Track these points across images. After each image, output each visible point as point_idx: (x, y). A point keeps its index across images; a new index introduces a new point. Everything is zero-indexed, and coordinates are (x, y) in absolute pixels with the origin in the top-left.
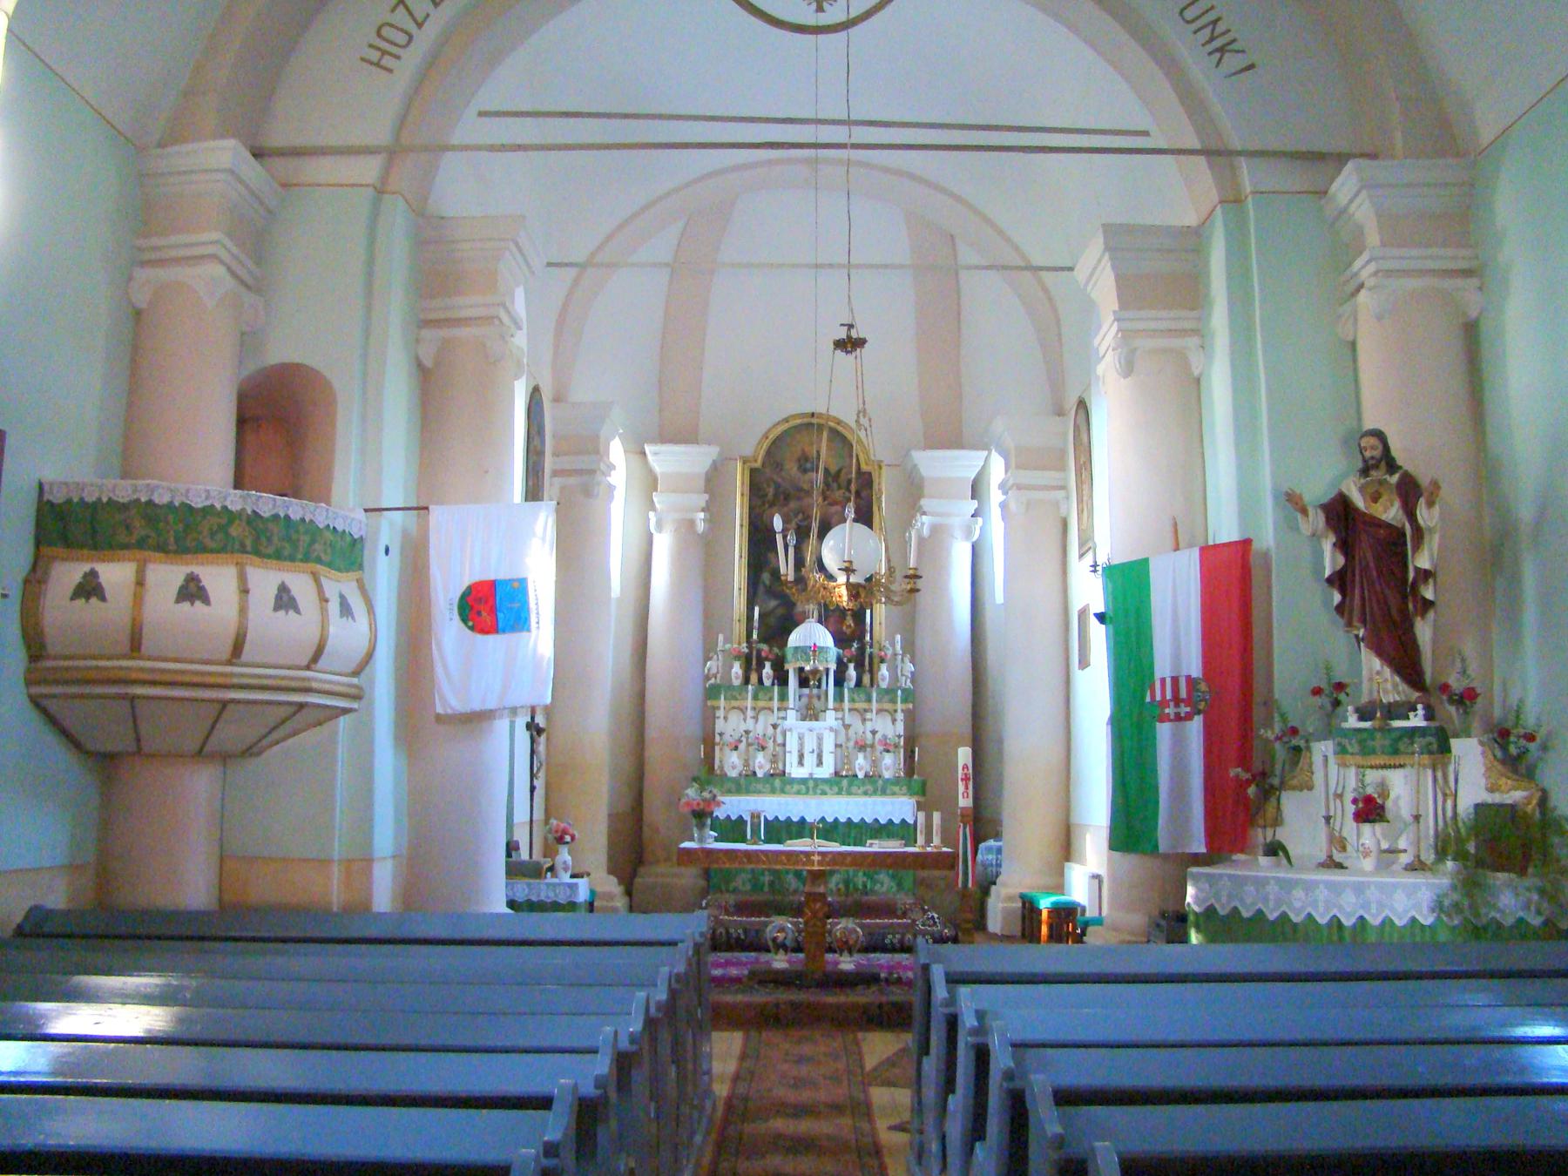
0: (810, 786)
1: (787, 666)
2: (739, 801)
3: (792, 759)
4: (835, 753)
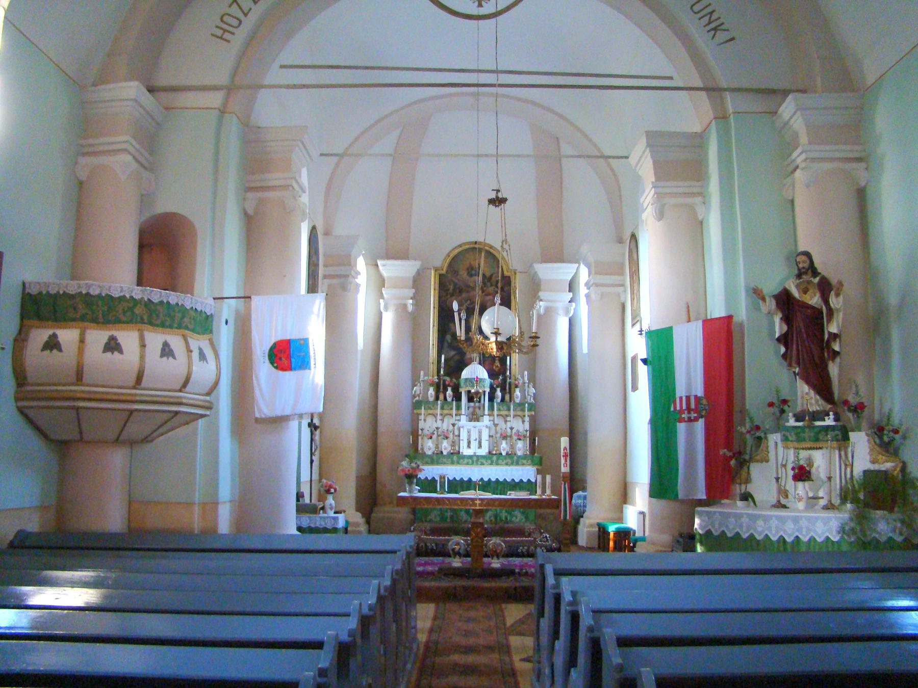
0: (475, 460)
1: (461, 390)
2: (433, 469)
3: (464, 444)
4: (489, 441)
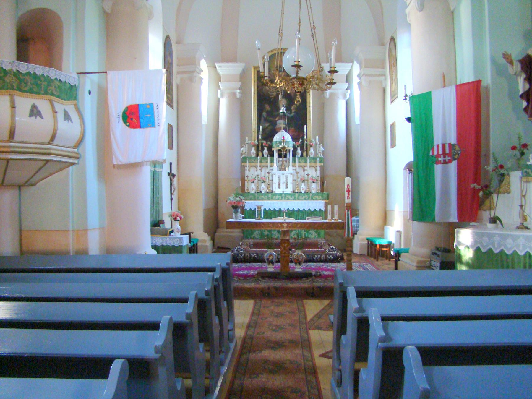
0: (283, 196)
1: (273, 149)
2: (255, 202)
3: (276, 186)
4: (293, 183)
